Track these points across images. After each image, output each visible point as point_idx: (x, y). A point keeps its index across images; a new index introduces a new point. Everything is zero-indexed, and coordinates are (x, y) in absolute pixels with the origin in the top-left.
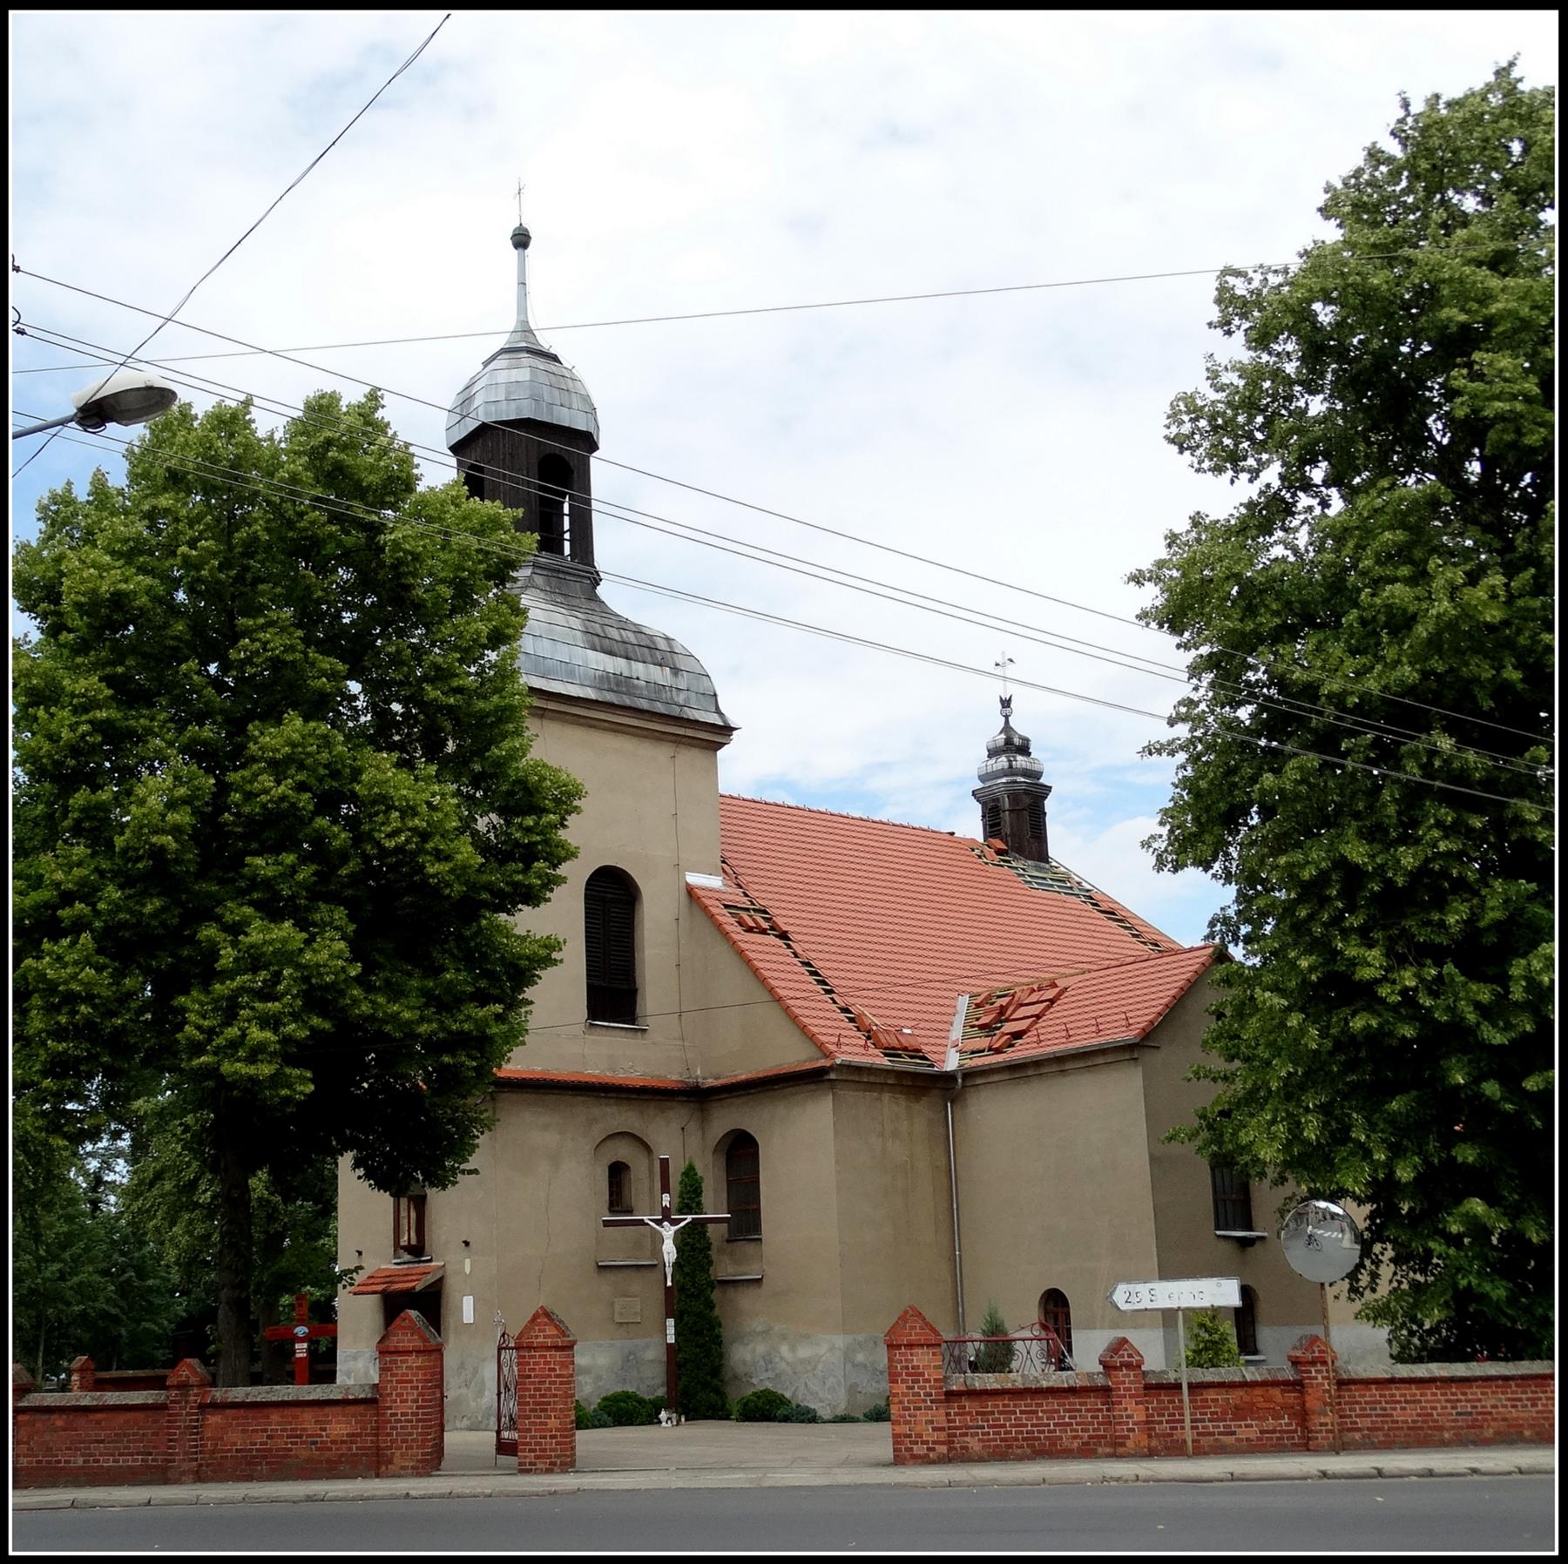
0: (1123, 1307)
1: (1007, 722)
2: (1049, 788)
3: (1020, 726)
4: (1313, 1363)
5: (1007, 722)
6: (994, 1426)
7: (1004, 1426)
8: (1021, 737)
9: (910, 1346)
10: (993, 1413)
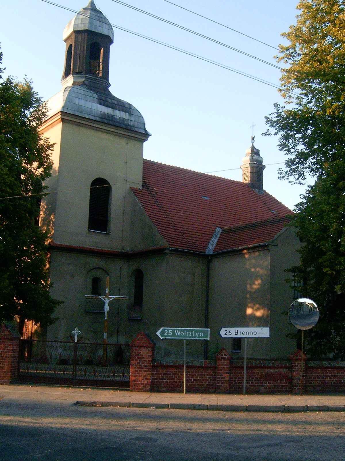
0: (224, 336)
1: (253, 145)
2: (265, 167)
3: (257, 147)
4: (297, 360)
5: (253, 145)
6: (170, 379)
7: (173, 379)
8: (256, 149)
9: (140, 347)
10: (170, 374)
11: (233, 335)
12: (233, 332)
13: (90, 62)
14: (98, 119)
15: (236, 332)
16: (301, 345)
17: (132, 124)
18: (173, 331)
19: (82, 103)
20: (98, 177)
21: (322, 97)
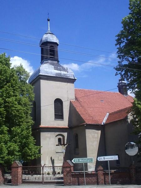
11: (103, 160)
12: (103, 158)
13: (46, 59)
14: (54, 76)
15: (104, 158)
16: (34, 166)
17: (68, 76)
18: (79, 160)
19: (48, 70)
20: (54, 100)
21: (17, 121)
